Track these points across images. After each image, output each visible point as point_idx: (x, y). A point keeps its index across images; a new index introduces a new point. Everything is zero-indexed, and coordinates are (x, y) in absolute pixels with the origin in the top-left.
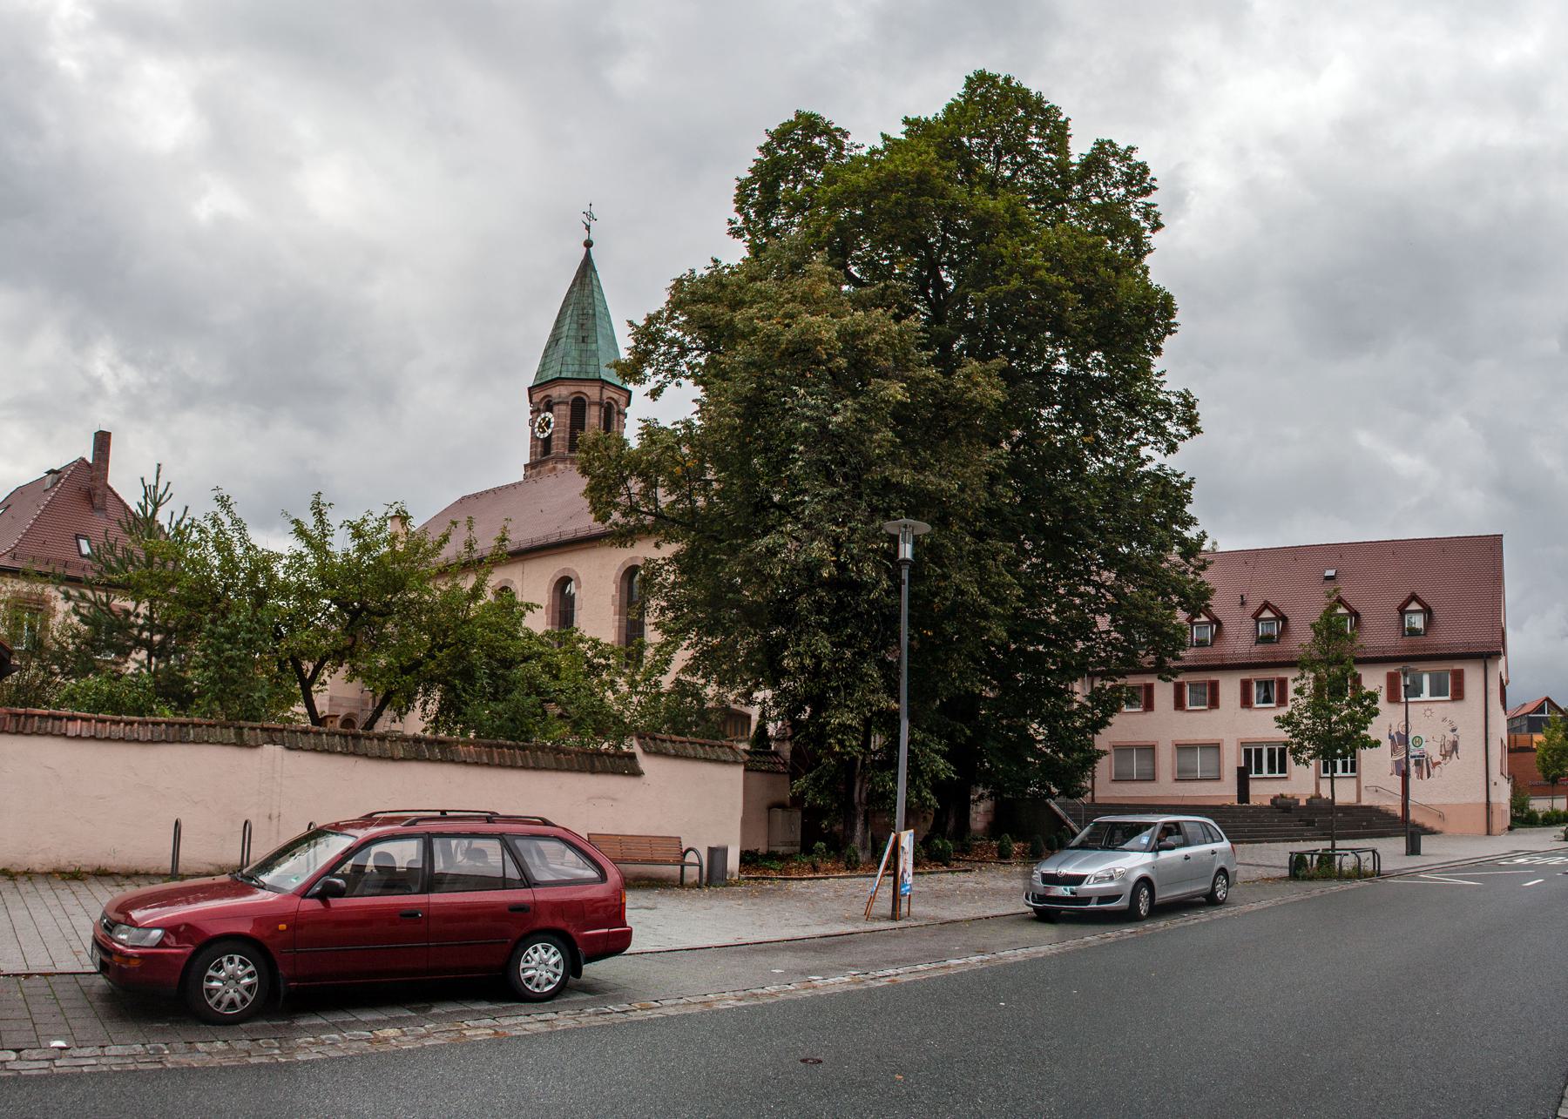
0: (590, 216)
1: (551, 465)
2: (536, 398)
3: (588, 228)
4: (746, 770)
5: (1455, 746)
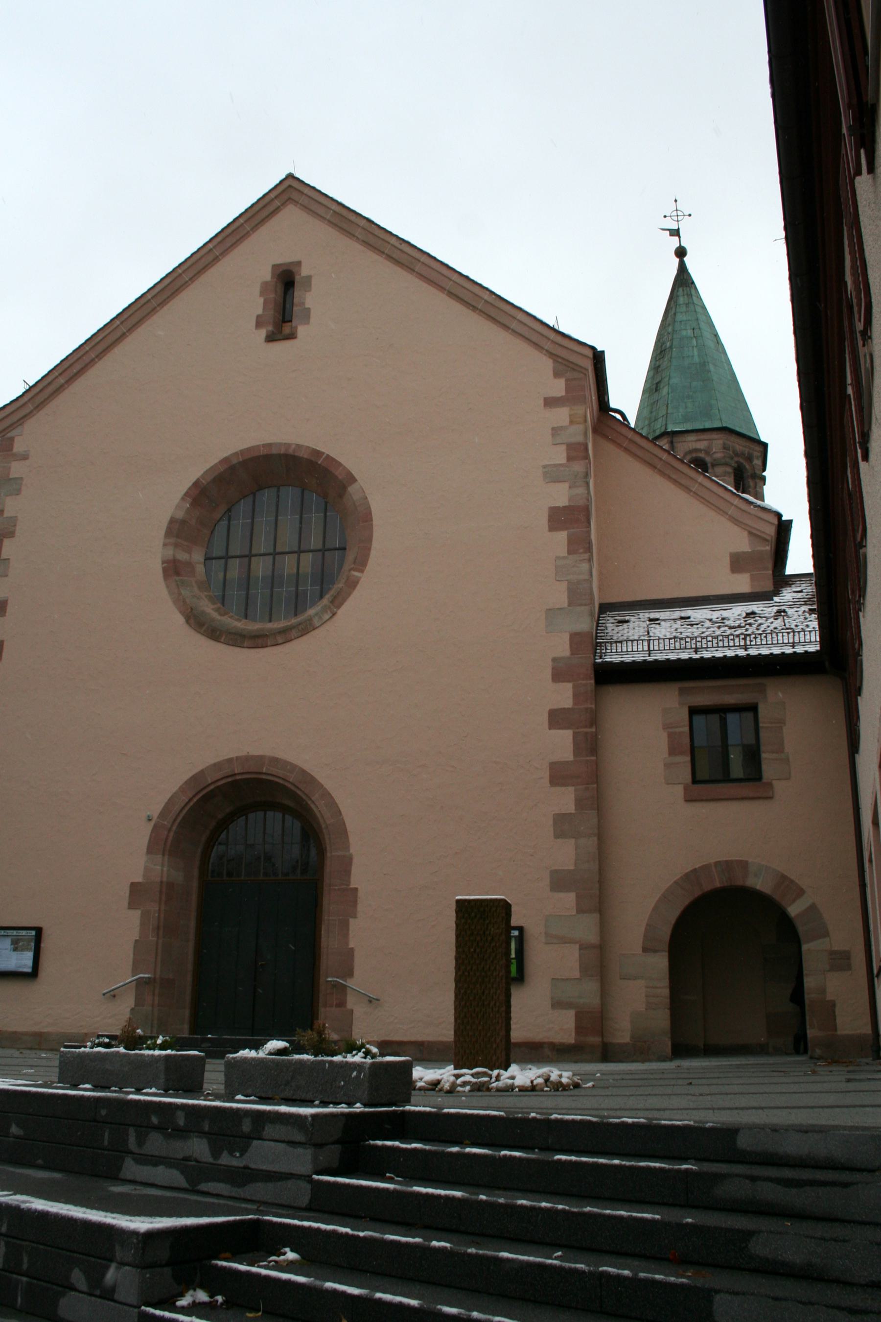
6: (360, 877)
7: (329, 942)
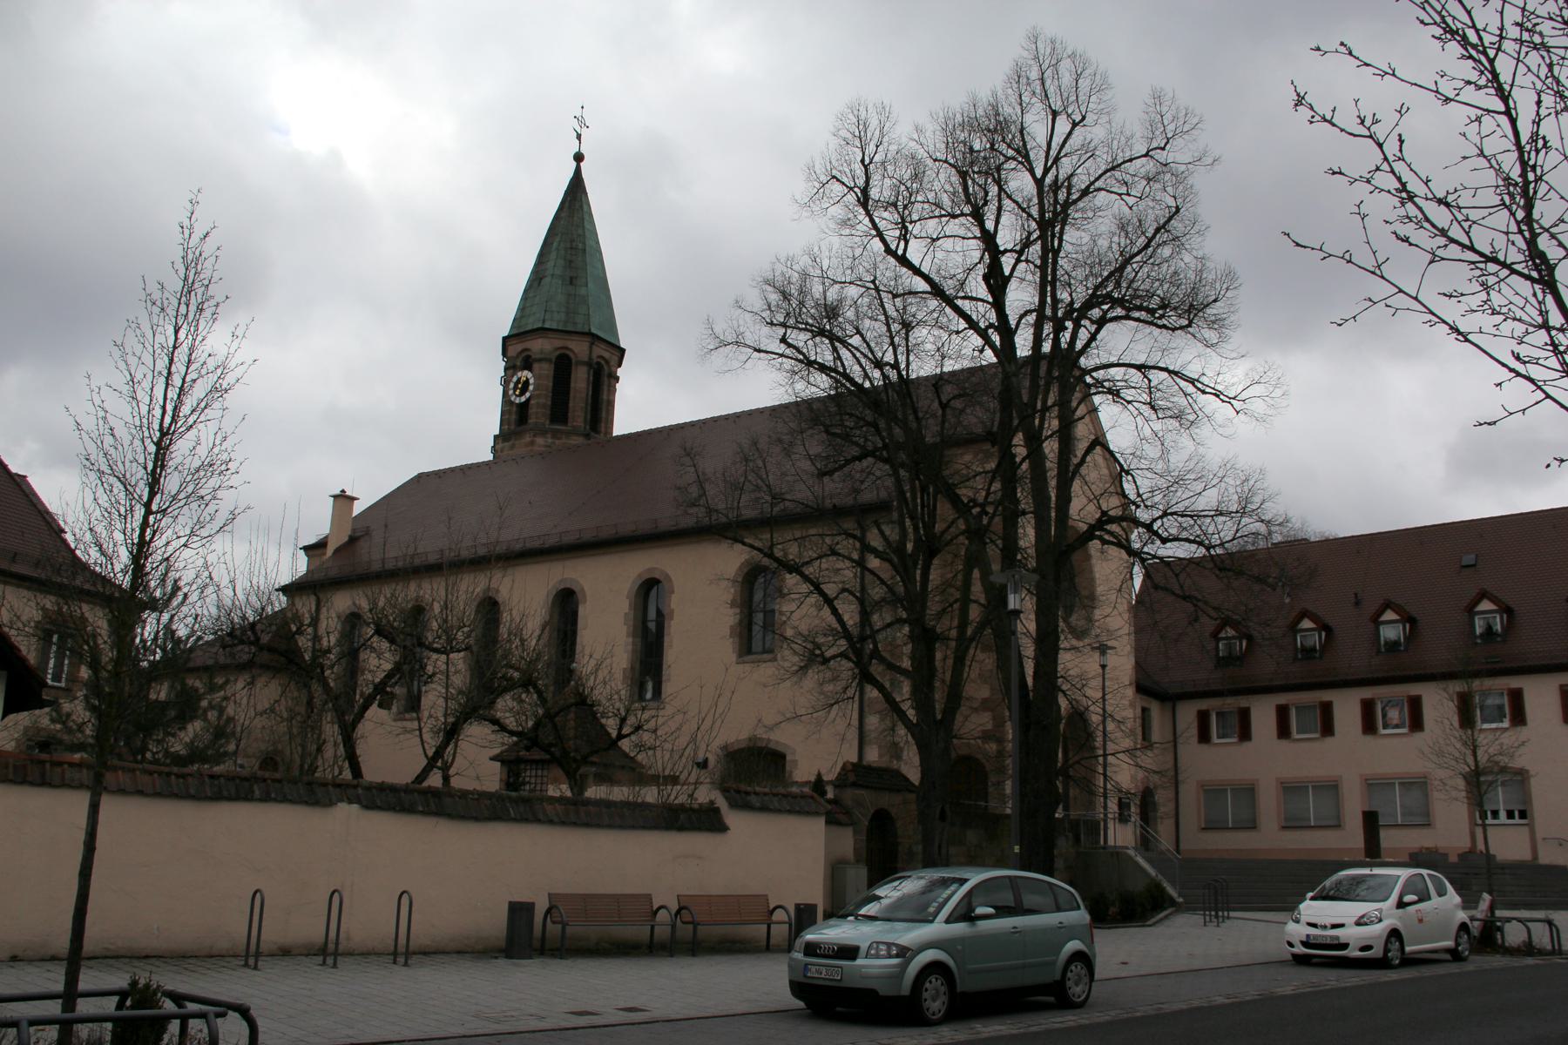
0: (581, 120)
1: (527, 439)
2: (512, 351)
3: (579, 137)
4: (827, 822)
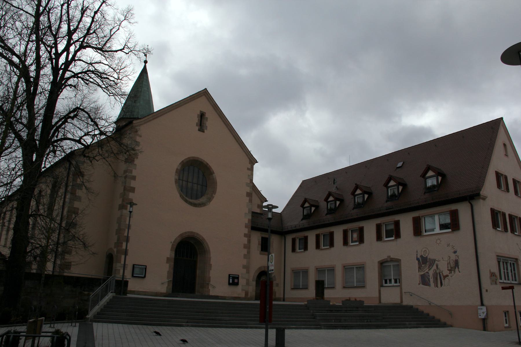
5: (457, 263)
6: (213, 262)
7: (171, 285)
